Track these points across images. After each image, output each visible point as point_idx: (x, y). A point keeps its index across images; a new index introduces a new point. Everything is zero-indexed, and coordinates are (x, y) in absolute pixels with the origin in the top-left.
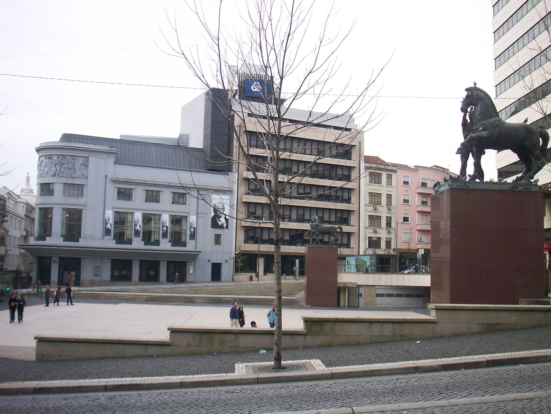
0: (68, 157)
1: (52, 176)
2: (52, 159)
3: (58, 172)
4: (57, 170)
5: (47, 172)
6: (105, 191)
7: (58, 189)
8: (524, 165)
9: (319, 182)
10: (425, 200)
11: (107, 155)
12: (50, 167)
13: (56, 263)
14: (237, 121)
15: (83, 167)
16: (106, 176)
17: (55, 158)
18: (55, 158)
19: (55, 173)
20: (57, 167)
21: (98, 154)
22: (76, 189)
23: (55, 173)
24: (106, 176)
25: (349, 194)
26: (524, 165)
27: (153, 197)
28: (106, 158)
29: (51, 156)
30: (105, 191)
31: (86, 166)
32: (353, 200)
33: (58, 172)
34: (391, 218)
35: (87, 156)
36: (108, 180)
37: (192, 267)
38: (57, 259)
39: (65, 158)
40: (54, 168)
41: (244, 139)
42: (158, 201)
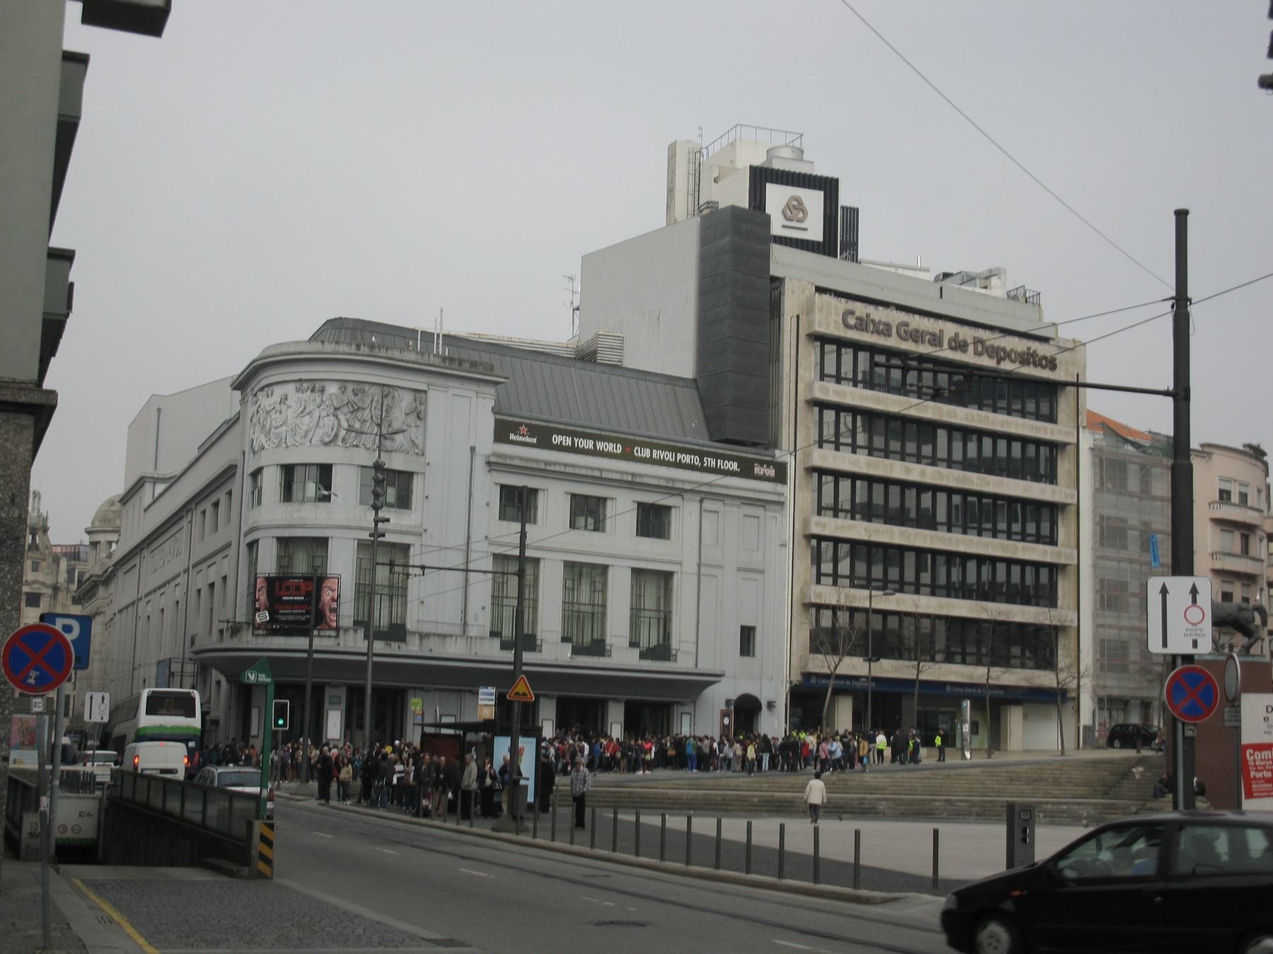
0: (374, 390)
1: (326, 444)
2: (322, 391)
3: (343, 433)
4: (339, 425)
5: (307, 432)
6: (470, 495)
7: (346, 483)
8: (482, 690)
9: (988, 484)
10: (1228, 588)
11: (475, 387)
12: (316, 415)
13: (339, 703)
14: (790, 306)
15: (412, 419)
16: (473, 449)
17: (332, 389)
18: (332, 389)
19: (336, 436)
20: (342, 417)
21: (449, 383)
22: (391, 486)
23: (336, 436)
24: (473, 449)
25: (1053, 524)
26: (482, 690)
27: (588, 511)
28: (473, 395)
29: (318, 385)
30: (470, 495)
31: (420, 416)
32: (1062, 534)
33: (343, 433)
34: (1246, 495)
35: (424, 387)
36: (479, 463)
37: (686, 720)
38: (342, 693)
39: (363, 391)
40: (332, 418)
41: (810, 355)
42: (504, 488)
